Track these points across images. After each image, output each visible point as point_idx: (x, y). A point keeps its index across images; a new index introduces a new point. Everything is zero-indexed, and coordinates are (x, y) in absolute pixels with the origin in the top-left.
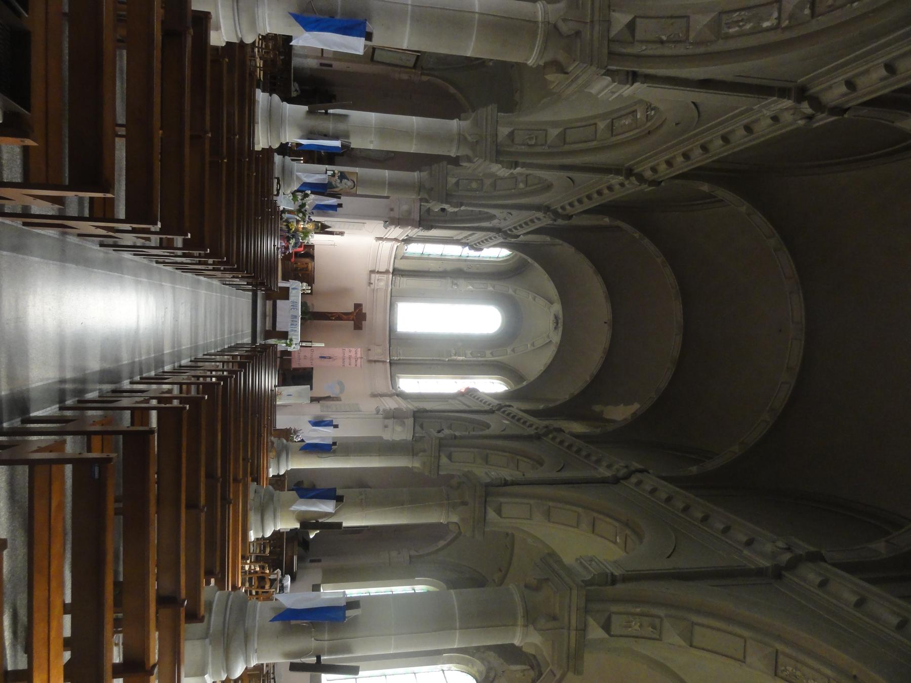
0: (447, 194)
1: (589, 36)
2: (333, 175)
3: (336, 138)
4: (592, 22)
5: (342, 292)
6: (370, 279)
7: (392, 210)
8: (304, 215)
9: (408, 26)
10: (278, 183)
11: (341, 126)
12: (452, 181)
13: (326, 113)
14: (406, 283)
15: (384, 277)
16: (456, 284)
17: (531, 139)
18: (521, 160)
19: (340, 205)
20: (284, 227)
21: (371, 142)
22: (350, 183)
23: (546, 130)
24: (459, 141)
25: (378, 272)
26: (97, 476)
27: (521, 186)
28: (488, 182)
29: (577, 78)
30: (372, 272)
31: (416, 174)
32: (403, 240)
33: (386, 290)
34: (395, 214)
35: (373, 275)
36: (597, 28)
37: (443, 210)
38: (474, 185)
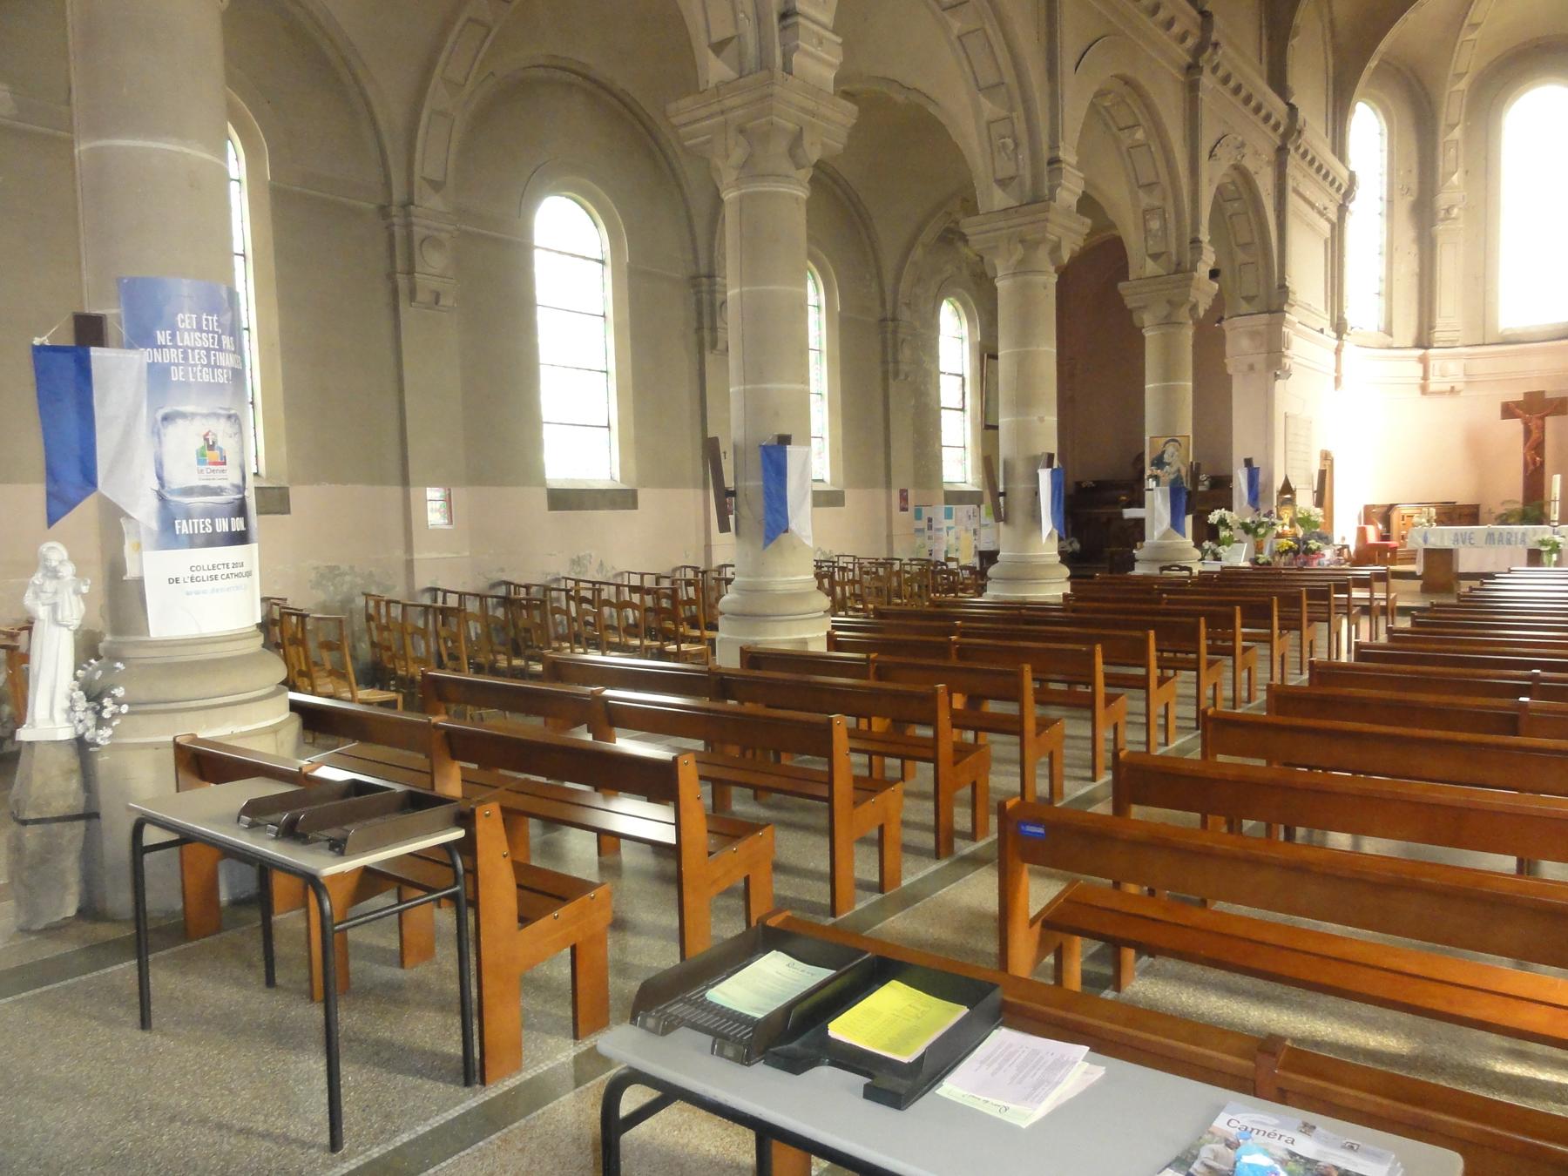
0: (1176, 272)
1: (740, 112)
2: (1156, 478)
3: (1036, 478)
4: (722, 112)
5: (1475, 445)
6: (1441, 393)
7: (1251, 367)
8: (1261, 524)
9: (769, 386)
10: (1169, 568)
11: (1021, 469)
12: (1151, 268)
13: (1004, 494)
14: (1450, 314)
15: (1435, 365)
16: (1448, 211)
17: (1004, 146)
18: (1045, 154)
19: (1248, 462)
20: (1284, 559)
21: (1042, 420)
22: (1170, 449)
23: (989, 123)
24: (1025, 273)
25: (1425, 377)
26: (1041, 830)
27: (1139, 135)
28: (1146, 200)
29: (803, 110)
30: (1424, 390)
31: (1149, 334)
32: (1339, 337)
33: (1470, 357)
34: (1260, 360)
35: (1432, 387)
36: (728, 103)
37: (1214, 274)
38: (1155, 225)
